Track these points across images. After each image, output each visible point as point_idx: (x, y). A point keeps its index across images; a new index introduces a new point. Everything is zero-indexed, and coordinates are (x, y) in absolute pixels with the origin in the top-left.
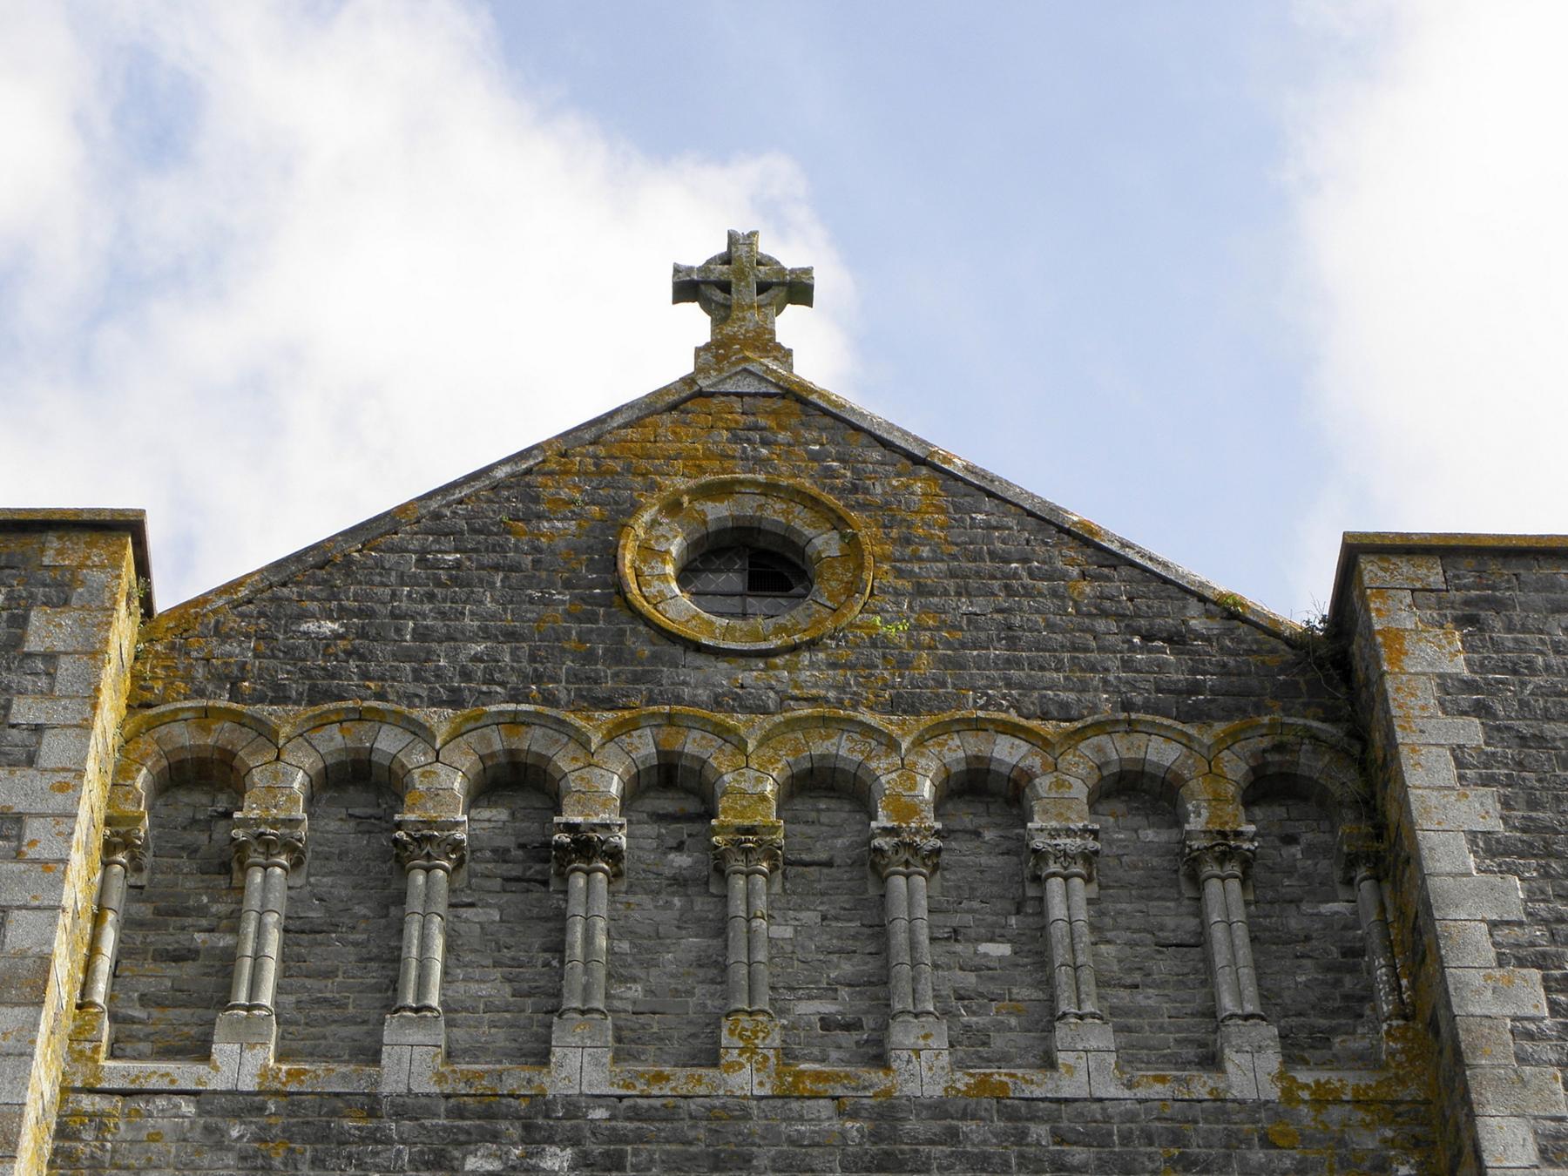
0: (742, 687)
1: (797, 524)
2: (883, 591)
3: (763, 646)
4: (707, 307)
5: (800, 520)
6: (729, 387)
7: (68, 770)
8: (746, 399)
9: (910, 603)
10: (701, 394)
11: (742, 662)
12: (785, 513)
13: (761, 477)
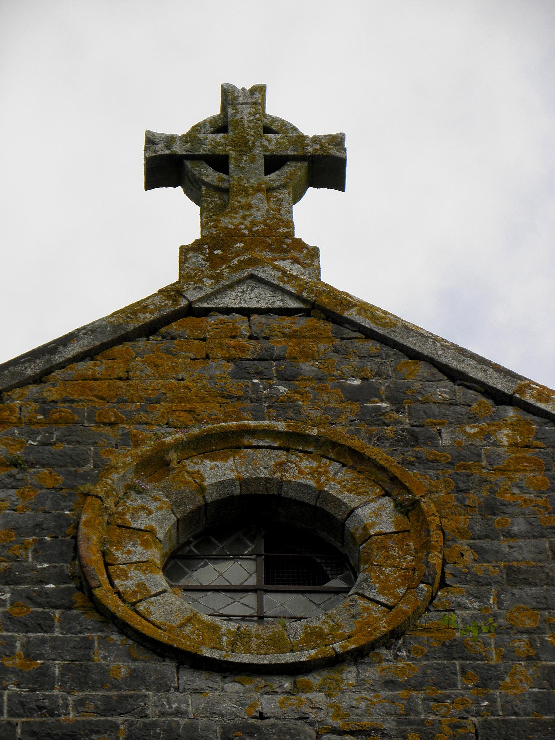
0: (261, 716)
1: (333, 489)
2: (459, 577)
3: (289, 658)
4: (194, 194)
5: (337, 483)
6: (229, 300)
7: (156, 595)
8: (255, 318)
9: (498, 596)
10: (191, 311)
11: (260, 681)
12: (315, 473)
13: (281, 426)
